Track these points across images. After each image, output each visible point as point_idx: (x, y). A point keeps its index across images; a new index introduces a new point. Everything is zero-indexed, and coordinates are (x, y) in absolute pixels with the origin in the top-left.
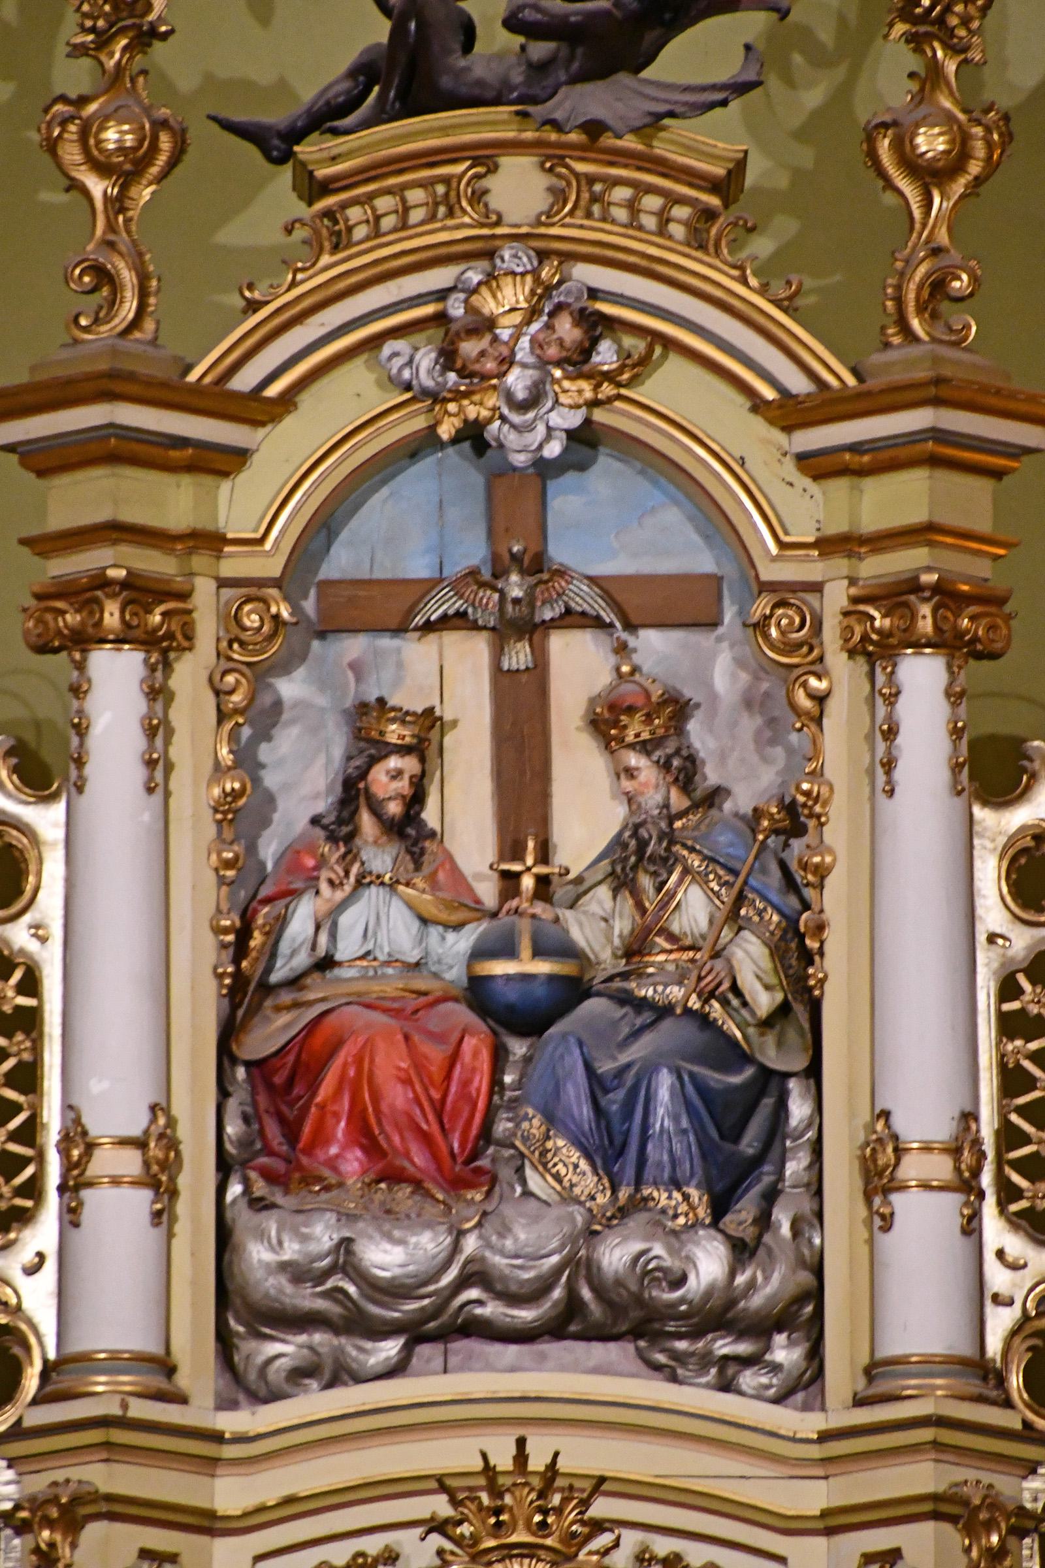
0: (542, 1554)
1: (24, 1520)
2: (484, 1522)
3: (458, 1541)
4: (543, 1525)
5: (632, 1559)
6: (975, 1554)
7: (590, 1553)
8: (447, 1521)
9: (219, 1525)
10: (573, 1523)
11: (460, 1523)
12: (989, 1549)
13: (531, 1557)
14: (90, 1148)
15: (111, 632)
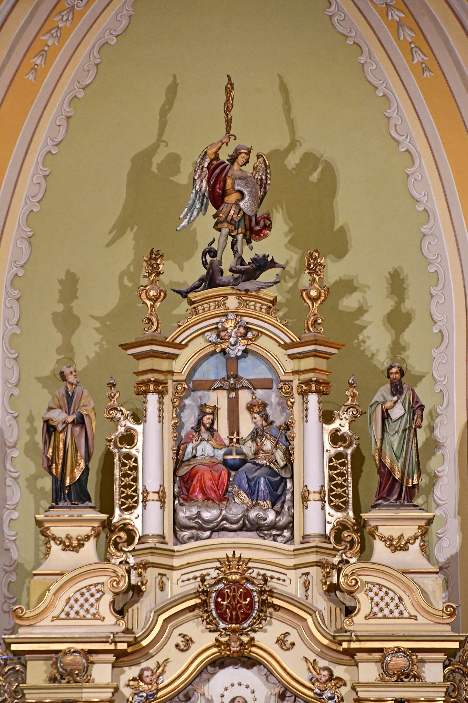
3: (221, 571)
4: (238, 568)
8: (219, 567)
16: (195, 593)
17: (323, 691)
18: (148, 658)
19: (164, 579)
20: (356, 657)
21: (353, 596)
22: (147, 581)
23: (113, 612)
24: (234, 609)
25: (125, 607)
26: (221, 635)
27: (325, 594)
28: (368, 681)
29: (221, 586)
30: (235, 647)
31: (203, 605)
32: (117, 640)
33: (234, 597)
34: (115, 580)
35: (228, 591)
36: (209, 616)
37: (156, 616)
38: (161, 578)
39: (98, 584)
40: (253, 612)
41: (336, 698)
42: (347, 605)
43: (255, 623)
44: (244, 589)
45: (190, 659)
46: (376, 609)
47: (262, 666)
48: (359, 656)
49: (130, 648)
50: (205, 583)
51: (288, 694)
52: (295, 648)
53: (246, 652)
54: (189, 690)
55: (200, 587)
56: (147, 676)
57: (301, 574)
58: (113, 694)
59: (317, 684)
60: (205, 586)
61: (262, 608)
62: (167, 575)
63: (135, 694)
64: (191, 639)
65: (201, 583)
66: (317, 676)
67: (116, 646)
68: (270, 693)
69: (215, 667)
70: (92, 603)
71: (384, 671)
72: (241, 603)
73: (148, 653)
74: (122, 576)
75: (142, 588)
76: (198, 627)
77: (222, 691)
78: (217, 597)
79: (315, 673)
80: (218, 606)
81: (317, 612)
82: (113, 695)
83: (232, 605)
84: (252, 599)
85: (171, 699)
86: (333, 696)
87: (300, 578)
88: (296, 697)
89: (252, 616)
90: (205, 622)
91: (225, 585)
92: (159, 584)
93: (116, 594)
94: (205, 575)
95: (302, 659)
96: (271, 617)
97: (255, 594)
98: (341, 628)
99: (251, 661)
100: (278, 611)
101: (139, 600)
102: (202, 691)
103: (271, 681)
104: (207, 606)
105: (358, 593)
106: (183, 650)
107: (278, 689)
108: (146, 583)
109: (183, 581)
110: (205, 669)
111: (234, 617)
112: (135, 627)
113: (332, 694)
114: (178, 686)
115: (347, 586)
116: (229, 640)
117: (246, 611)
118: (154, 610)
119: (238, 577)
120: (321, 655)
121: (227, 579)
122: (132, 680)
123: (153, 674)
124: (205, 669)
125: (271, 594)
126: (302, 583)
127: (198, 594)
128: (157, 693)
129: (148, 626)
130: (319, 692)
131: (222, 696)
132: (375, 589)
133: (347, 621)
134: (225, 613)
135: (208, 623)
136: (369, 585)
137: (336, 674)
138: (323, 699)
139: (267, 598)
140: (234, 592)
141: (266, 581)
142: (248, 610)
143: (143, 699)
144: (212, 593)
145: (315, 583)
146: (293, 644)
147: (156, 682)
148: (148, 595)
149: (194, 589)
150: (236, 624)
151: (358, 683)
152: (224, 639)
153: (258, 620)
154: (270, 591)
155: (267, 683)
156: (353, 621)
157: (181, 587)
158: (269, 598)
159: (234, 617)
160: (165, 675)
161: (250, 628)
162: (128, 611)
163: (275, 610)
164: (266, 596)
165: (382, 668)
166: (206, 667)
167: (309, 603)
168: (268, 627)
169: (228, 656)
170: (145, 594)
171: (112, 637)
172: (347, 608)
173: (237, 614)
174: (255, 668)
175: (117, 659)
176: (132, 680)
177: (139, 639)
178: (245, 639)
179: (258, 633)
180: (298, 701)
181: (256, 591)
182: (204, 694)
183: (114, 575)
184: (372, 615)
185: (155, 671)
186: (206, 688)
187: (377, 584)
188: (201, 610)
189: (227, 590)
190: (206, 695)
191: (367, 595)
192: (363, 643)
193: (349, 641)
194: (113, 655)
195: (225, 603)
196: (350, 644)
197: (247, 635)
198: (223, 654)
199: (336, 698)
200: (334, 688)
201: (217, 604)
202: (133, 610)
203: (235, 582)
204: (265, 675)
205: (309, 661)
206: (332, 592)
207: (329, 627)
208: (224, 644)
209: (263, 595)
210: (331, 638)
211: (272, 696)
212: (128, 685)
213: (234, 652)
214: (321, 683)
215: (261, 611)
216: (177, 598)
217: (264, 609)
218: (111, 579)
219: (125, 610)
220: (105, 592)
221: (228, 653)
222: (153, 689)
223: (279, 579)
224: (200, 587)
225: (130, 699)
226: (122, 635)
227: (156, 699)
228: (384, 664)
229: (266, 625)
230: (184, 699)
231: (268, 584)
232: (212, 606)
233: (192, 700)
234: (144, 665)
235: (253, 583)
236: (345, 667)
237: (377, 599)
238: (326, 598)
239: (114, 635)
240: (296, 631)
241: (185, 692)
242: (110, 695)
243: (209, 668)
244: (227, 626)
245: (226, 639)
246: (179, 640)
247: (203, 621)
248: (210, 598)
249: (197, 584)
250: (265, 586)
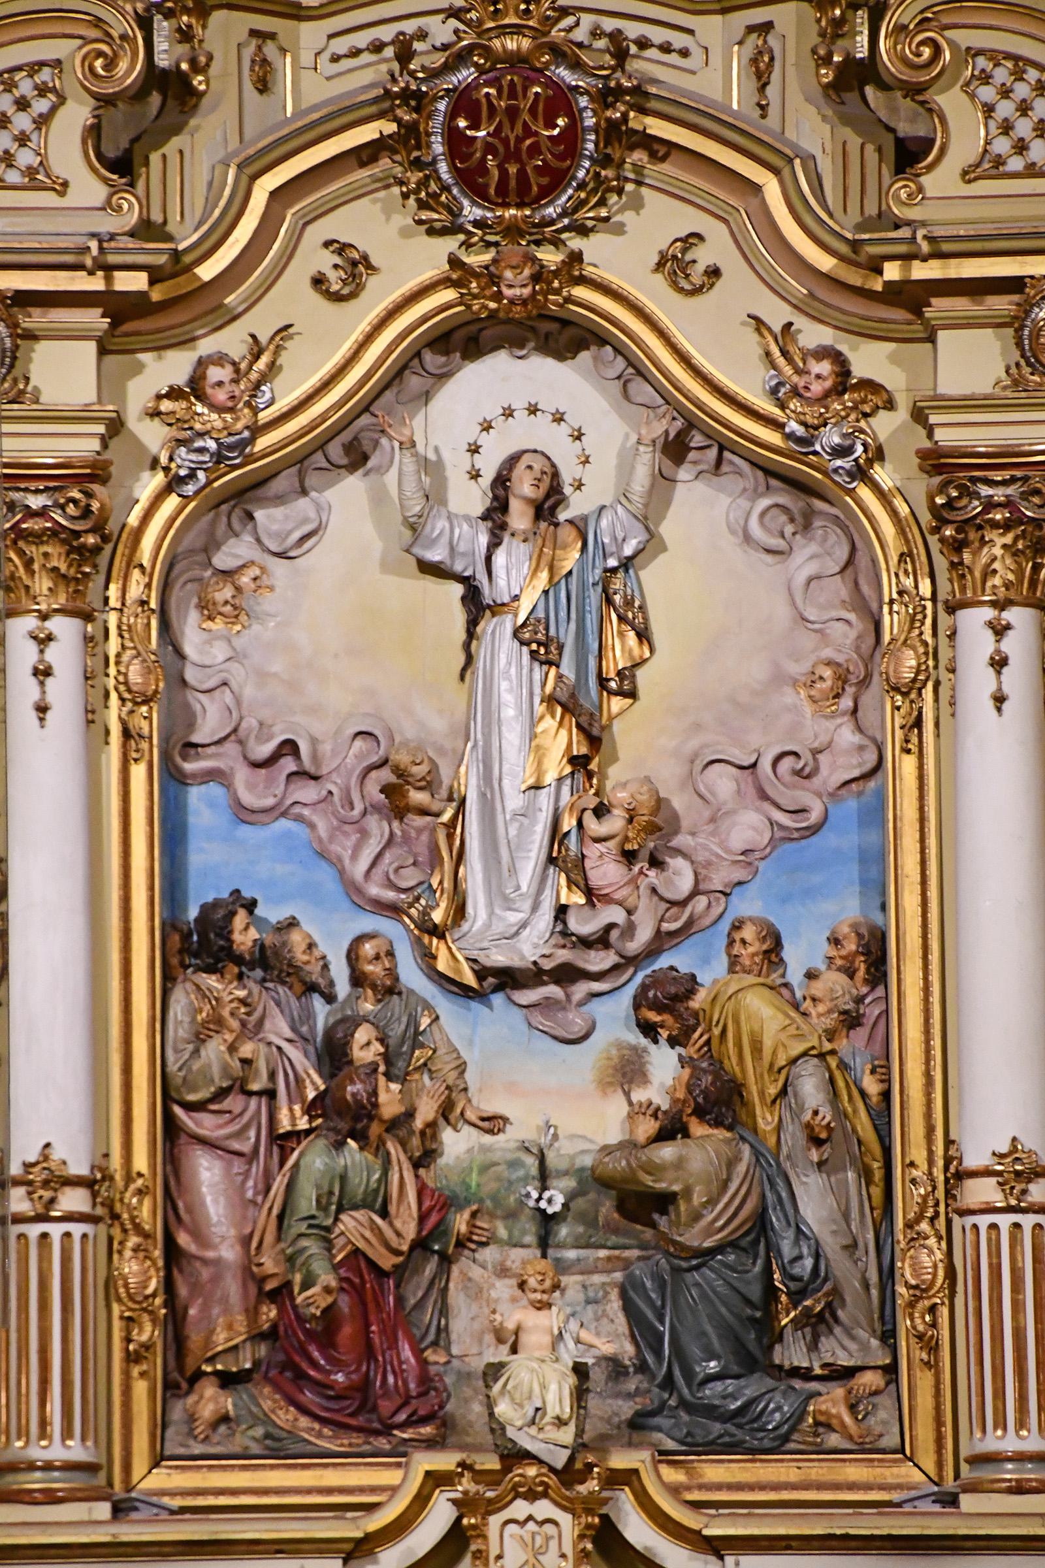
0: (527, 32)
1: (169, 8)
2: (486, 10)
3: (468, 23)
4: (527, 11)
5: (588, 34)
6: (823, 23)
7: (560, 30)
8: (460, 10)
9: (303, 13)
10: (548, 9)
11: (469, 11)
12: (834, 19)
13: (517, 33)
16: (376, 100)
17: (816, 428)
18: (218, 323)
19: (270, 49)
20: (928, 313)
21: (922, 103)
22: (210, 58)
23: (98, 165)
24: (513, 155)
25: (136, 146)
26: (467, 245)
27: (827, 96)
28: (967, 391)
29: (466, 75)
30: (516, 286)
31: (406, 144)
32: (112, 259)
33: (512, 113)
34: (100, 54)
35: (492, 91)
36: (427, 178)
37: (244, 180)
38: (259, 48)
39: (42, 64)
40: (579, 166)
41: (860, 449)
42: (901, 134)
43: (582, 203)
44: (545, 86)
45: (364, 326)
46: (1002, 146)
47: (608, 348)
48: (939, 307)
49: (158, 287)
50: (412, 67)
51: (697, 440)
52: (719, 284)
53: (555, 303)
54: (362, 430)
55: (394, 80)
56: (220, 384)
57: (742, 31)
58: (105, 441)
59: (794, 404)
60: (412, 74)
61: (609, 151)
62: (281, 36)
63: (180, 442)
64: (365, 258)
65: (396, 66)
66: (795, 378)
67: (109, 279)
68: (634, 438)
69: (447, 353)
70: (23, 133)
71: (1023, 356)
72: (536, 134)
73: (221, 305)
74: (124, 37)
75: (195, 83)
76: (388, 219)
77: (472, 433)
78: (452, 115)
79: (788, 370)
80: (456, 143)
81: (797, 162)
82: (105, 446)
83: (506, 142)
84: (575, 119)
85: (301, 461)
86: (848, 442)
87: (740, 43)
88: (722, 448)
89: (574, 177)
90: (412, 201)
91: (481, 70)
92: (252, 70)
93: (105, 101)
94: (412, 38)
95: (743, 324)
96: (639, 183)
97: (583, 101)
98: (880, 215)
99: (570, 332)
100: (663, 159)
101: (186, 123)
102: (407, 432)
103: (639, 400)
104: (418, 147)
105: (943, 91)
106: (337, 298)
107: (662, 426)
108: (208, 65)
109: (335, 59)
110: (416, 361)
111: (513, 183)
112: (174, 216)
113: (845, 436)
114: (323, 417)
115: (904, 69)
116: (495, 261)
117: (554, 163)
118: (237, 160)
119: (526, 43)
120: (809, 308)
121: (487, 51)
122: (168, 396)
123: (238, 375)
124: (416, 361)
125: (640, 100)
126: (745, 60)
127: (386, 105)
128: (252, 440)
129: (217, 212)
130: (800, 430)
131: (474, 449)
132: (1001, 75)
133: (901, 189)
134: (482, 169)
135: (422, 205)
136: (981, 62)
137: (860, 369)
138: (815, 453)
139: (625, 116)
140: (512, 95)
141: (621, 55)
142: (561, 157)
143: (206, 458)
144: (436, 98)
145: (791, 58)
146: (714, 273)
147: (248, 404)
148: (214, 108)
149: (372, 86)
150: (520, 206)
151: (936, 398)
152: (477, 259)
153: (594, 191)
154: (637, 91)
155: (626, 403)
156: (920, 189)
157: (328, 79)
158: (632, 114)
159: (513, 183)
160: (279, 382)
161: (566, 221)
162: (147, 163)
163: (654, 156)
164: (623, 108)
165: (1019, 344)
166: (418, 354)
167: (768, 131)
168: (628, 217)
169: (493, 314)
170: (205, 102)
171: (95, 251)
172: (900, 143)
173: (522, 173)
174: (585, 356)
175: (114, 325)
176: (168, 396)
177: (187, 259)
178: (550, 257)
179: (595, 238)
180: (731, 463)
181: (587, 92)
182: (413, 444)
183: (94, 33)
184: (986, 166)
185: (243, 366)
186: (418, 422)
187: (1009, 56)
188: (398, 158)
189: (486, 90)
190: (420, 447)
191: (972, 96)
192: (953, 262)
193: (907, 258)
194: (99, 311)
195: (482, 134)
196: (907, 269)
197: (557, 243)
198: (475, 308)
199: (860, 449)
200: (853, 417)
201: (455, 140)
202: (164, 156)
203: (516, 60)
204: (619, 377)
205: (769, 329)
206: (849, 89)
207: (839, 213)
208: (477, 276)
209: (612, 106)
210: (844, 249)
211: (642, 448)
212: (155, 414)
213: (512, 302)
214: (809, 402)
215: (605, 161)
216: (315, 116)
217: (616, 153)
218: (85, 50)
219: (137, 159)
220: (67, 93)
221: (493, 305)
222: (239, 426)
223: (666, 48)
224: (394, 80)
225: (164, 460)
226: (130, 243)
227: (250, 459)
228: (1026, 332)
229: (621, 210)
230: (345, 461)
231: (627, 67)
232: (438, 147)
233: (370, 464)
234: (207, 346)
235: (576, 65)
236: (893, 345)
237: (1005, 109)
238: (829, 113)
239: (100, 242)
240: (723, 226)
241: (346, 436)
242: (95, 445)
243: (428, 356)
244: (489, 215)
245: (487, 257)
246: (326, 261)
247: (405, 196)
248: (430, 117)
249: (384, 68)
250: (618, 74)
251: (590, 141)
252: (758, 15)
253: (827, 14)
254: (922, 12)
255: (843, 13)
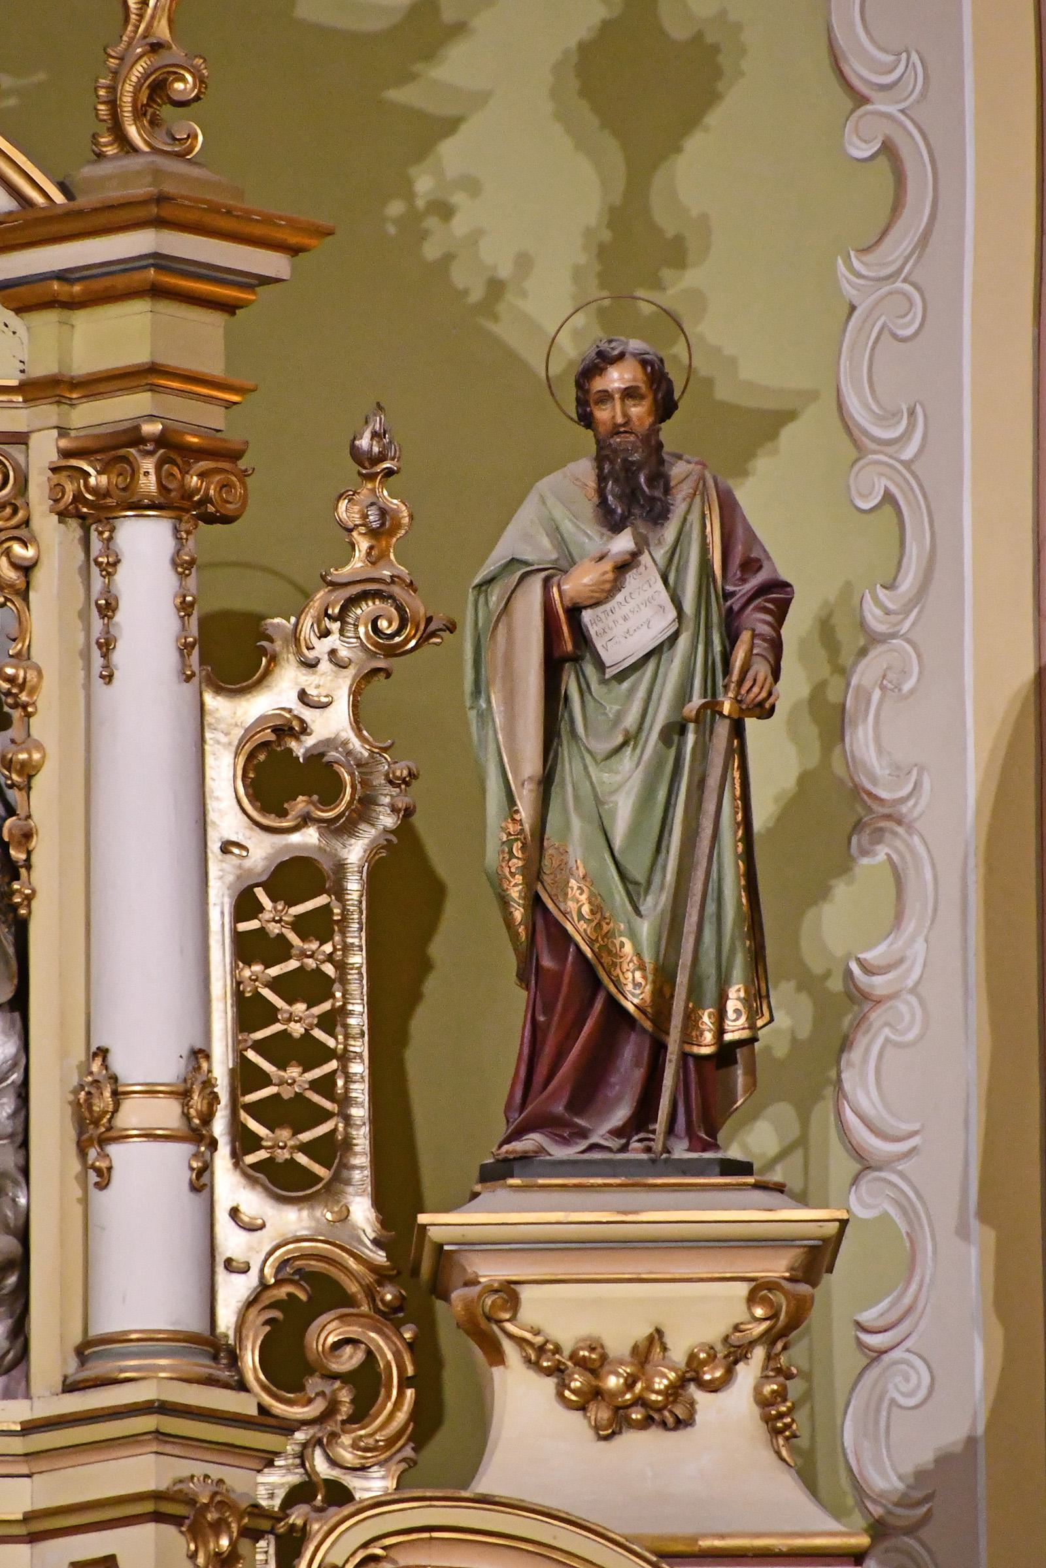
6: (201, 1560)
14: (118, 1096)
15: (148, 496)
251: (338, 915)
252: (367, 1079)
253: (206, 1544)
254: (365, 1545)
255: (233, 1544)
